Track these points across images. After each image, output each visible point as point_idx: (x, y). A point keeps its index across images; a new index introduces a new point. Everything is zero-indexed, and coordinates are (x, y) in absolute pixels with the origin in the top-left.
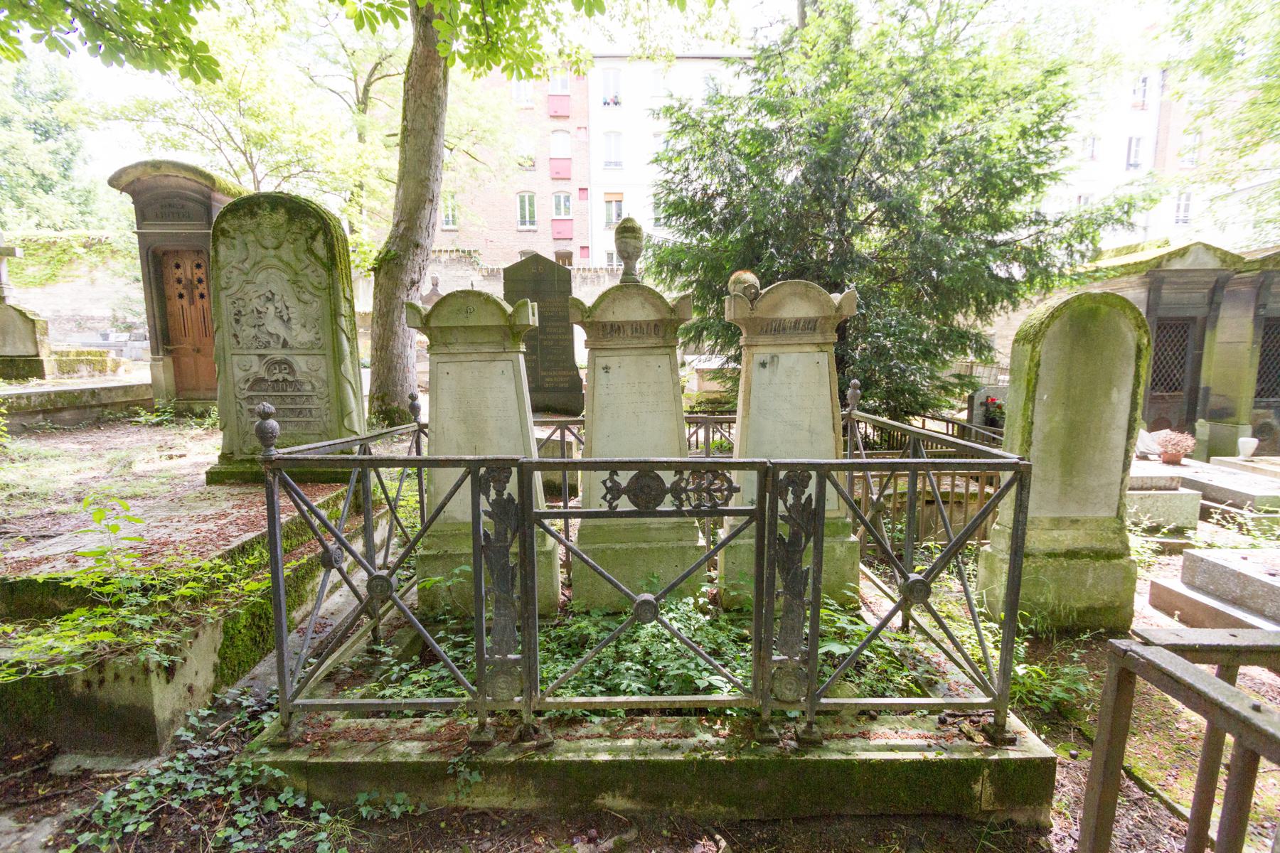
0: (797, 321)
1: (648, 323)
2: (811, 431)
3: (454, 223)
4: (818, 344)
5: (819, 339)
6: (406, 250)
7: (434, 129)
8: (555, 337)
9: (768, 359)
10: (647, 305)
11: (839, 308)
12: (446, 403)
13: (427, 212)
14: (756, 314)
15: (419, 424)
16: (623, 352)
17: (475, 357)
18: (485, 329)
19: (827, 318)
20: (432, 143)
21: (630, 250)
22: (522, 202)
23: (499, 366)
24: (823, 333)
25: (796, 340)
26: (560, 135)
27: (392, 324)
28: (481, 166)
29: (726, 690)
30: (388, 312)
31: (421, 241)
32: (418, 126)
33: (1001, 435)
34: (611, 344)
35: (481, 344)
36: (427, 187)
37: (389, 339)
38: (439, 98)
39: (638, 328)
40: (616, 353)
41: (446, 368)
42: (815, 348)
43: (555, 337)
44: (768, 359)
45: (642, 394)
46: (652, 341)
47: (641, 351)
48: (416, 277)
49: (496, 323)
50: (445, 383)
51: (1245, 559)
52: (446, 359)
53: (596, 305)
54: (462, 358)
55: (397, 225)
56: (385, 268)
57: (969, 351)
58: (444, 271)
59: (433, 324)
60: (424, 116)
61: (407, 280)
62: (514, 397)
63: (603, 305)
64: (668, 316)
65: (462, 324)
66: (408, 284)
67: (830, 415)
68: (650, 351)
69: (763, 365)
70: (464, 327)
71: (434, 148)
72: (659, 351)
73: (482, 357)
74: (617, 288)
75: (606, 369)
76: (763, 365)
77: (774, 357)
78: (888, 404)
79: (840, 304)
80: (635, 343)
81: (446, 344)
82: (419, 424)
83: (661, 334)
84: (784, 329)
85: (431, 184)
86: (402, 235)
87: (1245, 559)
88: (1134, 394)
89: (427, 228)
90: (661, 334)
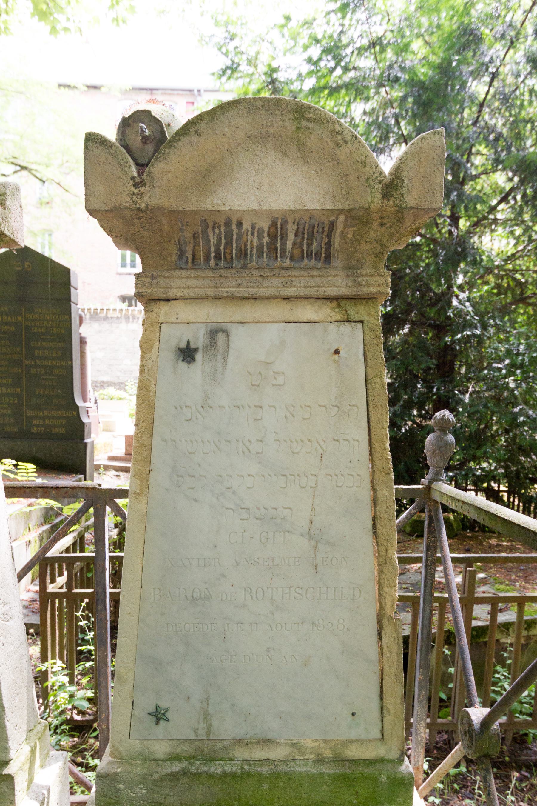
0: (277, 229)
2: (314, 536)
4: (338, 300)
5: (338, 284)
8: (48, 363)
9: (200, 339)
11: (392, 186)
14: (152, 198)
19: (359, 218)
24: (352, 268)
25: (274, 285)
33: (176, 104)
42: (327, 311)
43: (48, 363)
44: (200, 339)
67: (366, 495)
69: (187, 354)
76: (187, 354)
77: (215, 333)
78: (506, 467)
79: (397, 170)
84: (243, 254)
88: (115, 612)
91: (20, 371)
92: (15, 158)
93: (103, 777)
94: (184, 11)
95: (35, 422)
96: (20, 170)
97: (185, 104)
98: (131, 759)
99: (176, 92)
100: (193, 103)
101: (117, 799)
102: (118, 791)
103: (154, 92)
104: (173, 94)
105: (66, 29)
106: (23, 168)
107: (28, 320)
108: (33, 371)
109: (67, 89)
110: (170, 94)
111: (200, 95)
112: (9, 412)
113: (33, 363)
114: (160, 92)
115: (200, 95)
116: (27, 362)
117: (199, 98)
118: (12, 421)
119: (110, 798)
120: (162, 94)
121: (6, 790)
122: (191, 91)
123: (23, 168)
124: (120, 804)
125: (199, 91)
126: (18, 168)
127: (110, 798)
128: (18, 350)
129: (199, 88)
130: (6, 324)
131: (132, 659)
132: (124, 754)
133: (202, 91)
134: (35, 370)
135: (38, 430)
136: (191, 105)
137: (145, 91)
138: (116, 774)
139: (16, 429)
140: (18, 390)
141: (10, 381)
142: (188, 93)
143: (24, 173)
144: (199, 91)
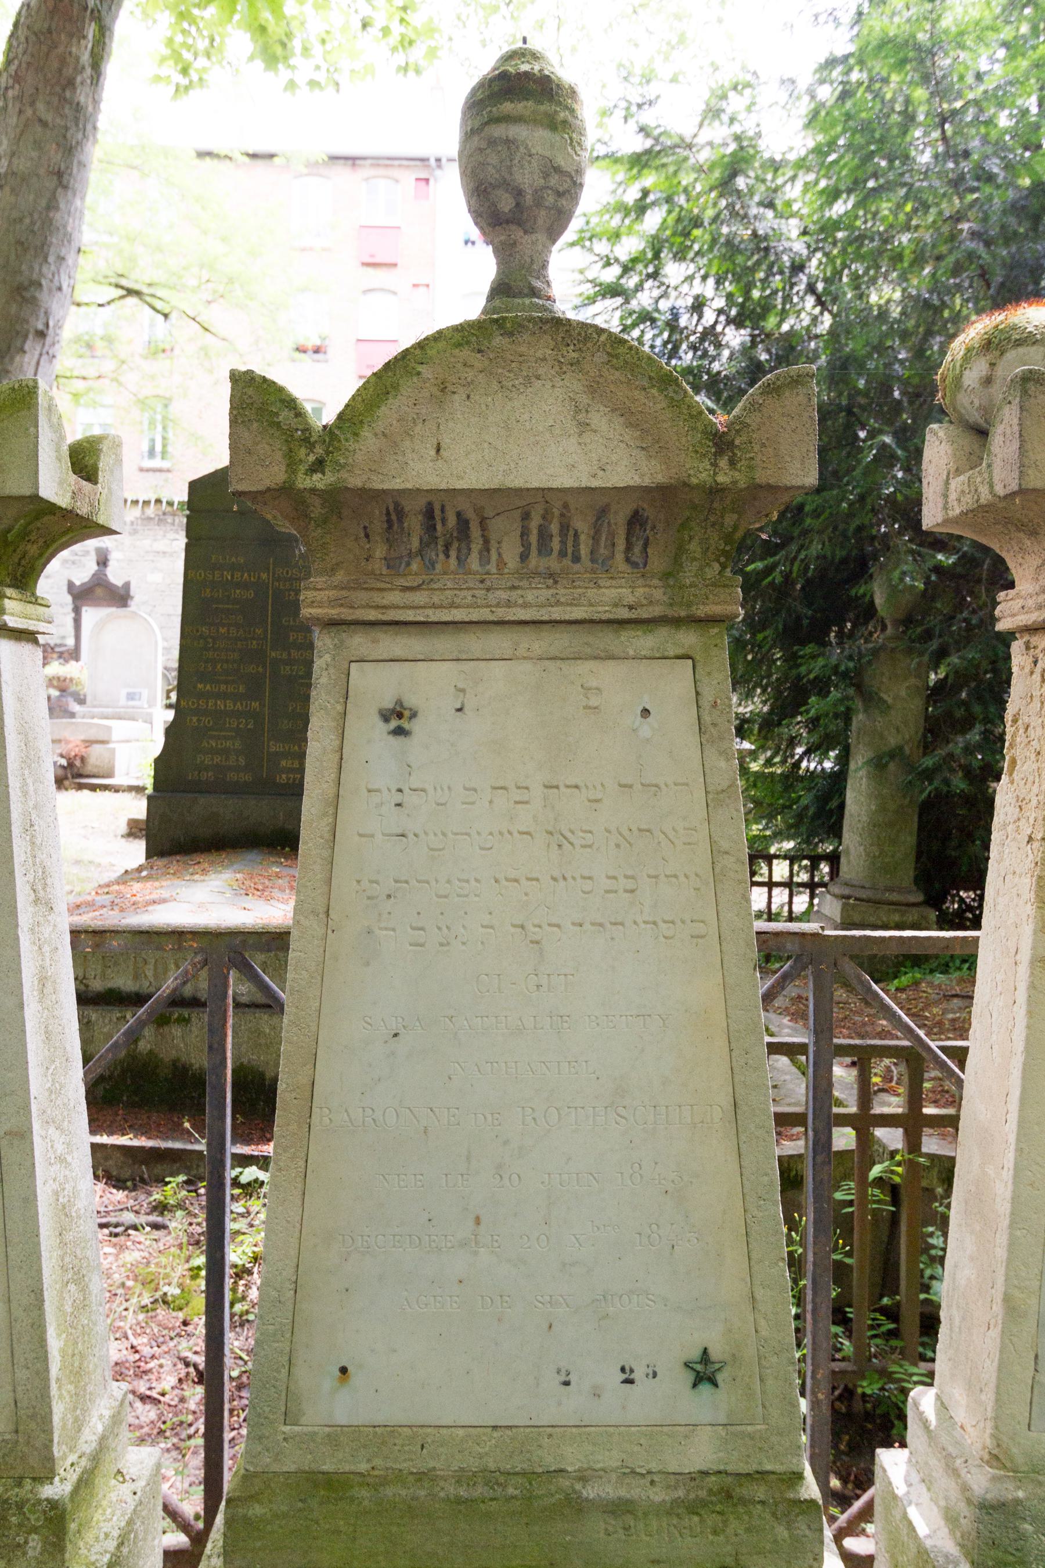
1: (599, 502)
3: (164, 454)
7: (59, 174)
10: (599, 418)
16: (474, 643)
20: (52, 205)
21: (527, 177)
32: (22, 165)
34: (416, 605)
36: (33, 302)
38: (78, 108)
39: (551, 526)
40: (444, 644)
45: (559, 839)
46: (614, 594)
47: (560, 641)
53: (351, 417)
60: (38, 145)
63: (388, 413)
64: (701, 473)
68: (607, 640)
71: (58, 216)
72: (645, 642)
74: (464, 336)
75: (398, 718)
80: (534, 600)
83: (657, 562)
85: (43, 296)
90: (657, 562)
91: (260, 669)
92: (122, 276)
93: (992, 1507)
94: (450, 39)
95: (283, 763)
96: (122, 297)
97: (413, 182)
98: (1034, 1472)
99: (381, 162)
100: (427, 180)
101: (1018, 1554)
102: (1022, 1537)
103: (358, 162)
104: (392, 166)
105: (313, 84)
106: (131, 292)
107: (279, 580)
108: (285, 670)
109: (208, 159)
110: (387, 166)
111: (439, 167)
112: (238, 744)
113: (285, 656)
114: (369, 162)
115: (439, 167)
116: (273, 654)
117: (438, 172)
118: (242, 761)
119: (1006, 1551)
120: (372, 165)
121: (807, 1532)
122: (424, 160)
123: (131, 292)
124: (1022, 1562)
125: (438, 160)
126: (124, 292)
127: (1006, 1551)
128: (259, 631)
129: (438, 156)
130: (238, 585)
131: (1036, 1271)
132: (1020, 1460)
133: (444, 161)
134: (288, 668)
135: (288, 779)
136: (423, 183)
137: (342, 162)
138: (1017, 1502)
139: (247, 777)
140: (255, 705)
141: (242, 689)
142: (418, 163)
143: (132, 300)
144: (438, 160)
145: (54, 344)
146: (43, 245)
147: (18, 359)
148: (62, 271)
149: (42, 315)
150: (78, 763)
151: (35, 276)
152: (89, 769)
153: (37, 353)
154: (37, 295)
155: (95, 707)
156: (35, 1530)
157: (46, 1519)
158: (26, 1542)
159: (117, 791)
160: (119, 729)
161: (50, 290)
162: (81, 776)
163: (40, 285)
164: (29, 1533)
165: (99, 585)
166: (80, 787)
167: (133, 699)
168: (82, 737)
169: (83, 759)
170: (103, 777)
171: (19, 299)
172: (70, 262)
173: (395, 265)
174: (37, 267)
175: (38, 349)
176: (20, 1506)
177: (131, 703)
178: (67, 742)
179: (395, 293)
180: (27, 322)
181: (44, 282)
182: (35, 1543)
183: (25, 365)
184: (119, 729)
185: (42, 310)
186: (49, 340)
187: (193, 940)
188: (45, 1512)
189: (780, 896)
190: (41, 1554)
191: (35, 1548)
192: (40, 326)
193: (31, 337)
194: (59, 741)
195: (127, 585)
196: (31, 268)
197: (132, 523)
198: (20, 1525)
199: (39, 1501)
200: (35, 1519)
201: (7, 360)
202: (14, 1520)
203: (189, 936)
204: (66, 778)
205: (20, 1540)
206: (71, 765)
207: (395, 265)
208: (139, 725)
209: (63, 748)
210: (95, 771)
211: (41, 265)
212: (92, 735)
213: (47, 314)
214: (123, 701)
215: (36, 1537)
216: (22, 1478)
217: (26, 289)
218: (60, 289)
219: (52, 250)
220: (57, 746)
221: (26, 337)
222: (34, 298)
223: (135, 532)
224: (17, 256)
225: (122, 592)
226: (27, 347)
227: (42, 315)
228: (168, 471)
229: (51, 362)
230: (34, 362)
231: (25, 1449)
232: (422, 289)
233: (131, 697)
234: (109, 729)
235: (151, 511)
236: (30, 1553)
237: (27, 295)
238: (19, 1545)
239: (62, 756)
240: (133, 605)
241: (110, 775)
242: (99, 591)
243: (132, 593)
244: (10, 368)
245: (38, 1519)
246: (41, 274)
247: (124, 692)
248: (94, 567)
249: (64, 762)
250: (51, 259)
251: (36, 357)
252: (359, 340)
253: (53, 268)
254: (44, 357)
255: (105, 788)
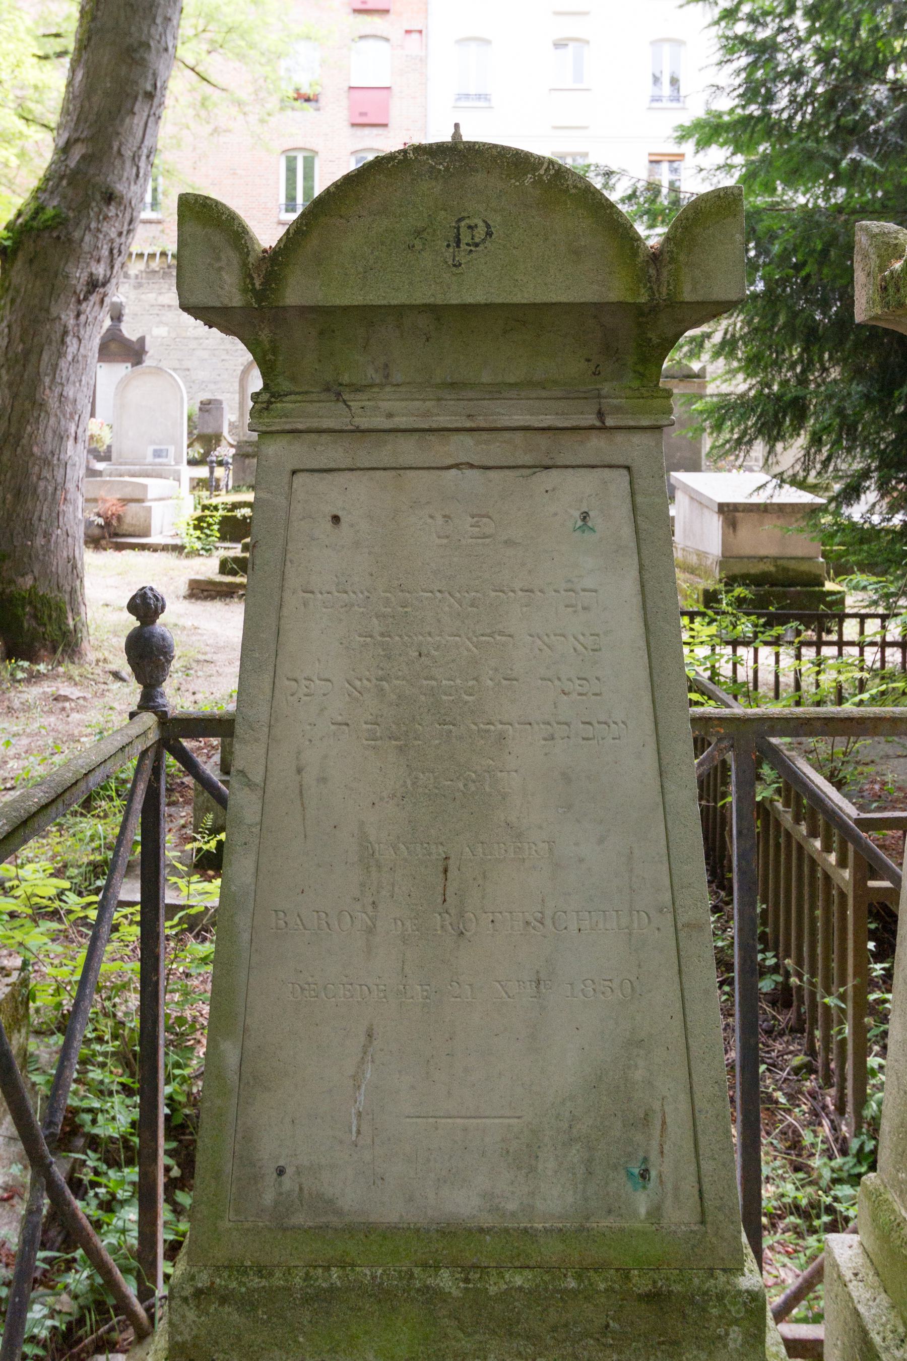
6: (85, 205)
12: (322, 648)
13: (138, 121)
15: (164, 720)
17: (463, 447)
18: (522, 321)
22: (291, 170)
23: (572, 490)
26: (371, 43)
27: (35, 383)
28: (216, 95)
29: (799, 1195)
30: (27, 353)
31: (120, 188)
35: (496, 391)
36: (142, 63)
37: (23, 420)
41: (331, 494)
48: (100, 270)
49: (588, 294)
50: (322, 563)
51: (336, 519)
52: (332, 453)
54: (407, 450)
55: (64, 150)
56: (29, 246)
57: (802, 432)
58: (133, 294)
59: (297, 291)
61: (79, 276)
62: (636, 629)
65: (424, 295)
66: (81, 287)
70: (436, 311)
73: (495, 450)
81: (336, 391)
82: (164, 720)
85: (152, 57)
86: (76, 172)
87: (336, 519)
89: (135, 158)
145: (160, 105)
146: (151, 6)
147: (127, 120)
148: (168, 32)
149: (150, 77)
150: (114, 522)
151: (144, 38)
152: (125, 528)
153: (146, 114)
154: (146, 55)
155: (121, 464)
156: (736, 1322)
157: (747, 1311)
158: (727, 1334)
159: (155, 550)
160: (154, 487)
161: (158, 52)
162: (117, 535)
163: (149, 46)
164: (729, 1325)
165: (113, 340)
166: (120, 547)
167: (159, 456)
168: (118, 496)
169: (119, 518)
170: (139, 536)
171: (130, 61)
172: (175, 22)
173: (387, 11)
174: (145, 29)
175: (147, 110)
176: (720, 1297)
177: (158, 460)
178: (105, 501)
179: (387, 40)
180: (136, 83)
181: (152, 44)
182: (736, 1335)
183: (135, 127)
184: (154, 487)
185: (151, 71)
186: (156, 101)
187: (720, 726)
188: (745, 1303)
189: (871, 655)
190: (742, 1346)
191: (735, 1341)
192: (149, 88)
193: (140, 98)
194: (95, 500)
195: (142, 340)
196: (140, 30)
197: (137, 276)
198: (721, 1317)
199: (739, 1293)
200: (737, 1311)
201: (118, 122)
202: (714, 1311)
203: (716, 722)
204: (104, 538)
205: (721, 1331)
206: (108, 524)
207: (387, 11)
208: (171, 482)
209: (100, 507)
210: (131, 529)
211: (149, 26)
212: (128, 493)
213: (155, 74)
214: (150, 459)
215: (736, 1328)
216: (712, 1269)
217: (135, 51)
218: (166, 50)
219: (160, 11)
220: (91, 505)
221: (136, 98)
222: (143, 59)
223: (139, 286)
224: (126, 18)
225: (137, 347)
226: (136, 109)
227: (150, 77)
228: (159, 222)
229: (157, 123)
230: (142, 124)
231: (714, 1240)
232: (415, 36)
233: (157, 454)
234: (145, 487)
235: (155, 264)
236: (731, 1345)
237: (137, 56)
238: (719, 1337)
239: (99, 515)
240: (148, 361)
241: (147, 534)
242: (113, 346)
243: (147, 349)
244: (121, 130)
245: (738, 1312)
246: (149, 35)
247: (150, 449)
248: (108, 323)
249: (101, 521)
250: (159, 20)
251: (145, 118)
252: (351, 88)
253: (160, 29)
254: (152, 119)
255: (143, 547)
